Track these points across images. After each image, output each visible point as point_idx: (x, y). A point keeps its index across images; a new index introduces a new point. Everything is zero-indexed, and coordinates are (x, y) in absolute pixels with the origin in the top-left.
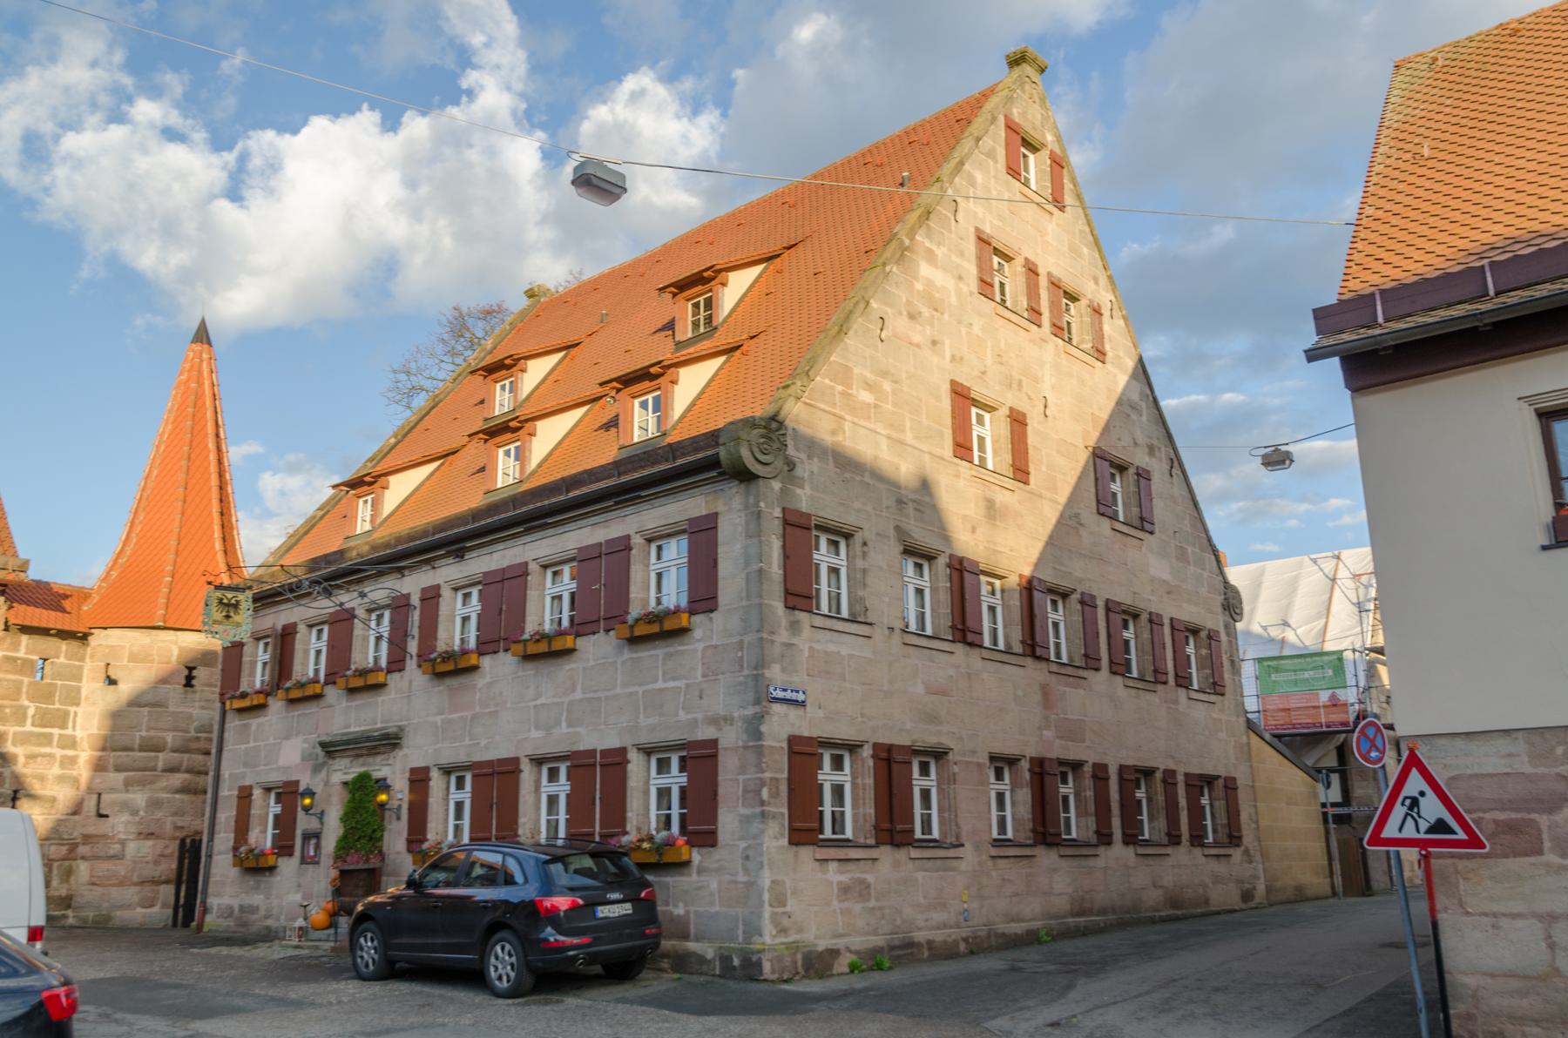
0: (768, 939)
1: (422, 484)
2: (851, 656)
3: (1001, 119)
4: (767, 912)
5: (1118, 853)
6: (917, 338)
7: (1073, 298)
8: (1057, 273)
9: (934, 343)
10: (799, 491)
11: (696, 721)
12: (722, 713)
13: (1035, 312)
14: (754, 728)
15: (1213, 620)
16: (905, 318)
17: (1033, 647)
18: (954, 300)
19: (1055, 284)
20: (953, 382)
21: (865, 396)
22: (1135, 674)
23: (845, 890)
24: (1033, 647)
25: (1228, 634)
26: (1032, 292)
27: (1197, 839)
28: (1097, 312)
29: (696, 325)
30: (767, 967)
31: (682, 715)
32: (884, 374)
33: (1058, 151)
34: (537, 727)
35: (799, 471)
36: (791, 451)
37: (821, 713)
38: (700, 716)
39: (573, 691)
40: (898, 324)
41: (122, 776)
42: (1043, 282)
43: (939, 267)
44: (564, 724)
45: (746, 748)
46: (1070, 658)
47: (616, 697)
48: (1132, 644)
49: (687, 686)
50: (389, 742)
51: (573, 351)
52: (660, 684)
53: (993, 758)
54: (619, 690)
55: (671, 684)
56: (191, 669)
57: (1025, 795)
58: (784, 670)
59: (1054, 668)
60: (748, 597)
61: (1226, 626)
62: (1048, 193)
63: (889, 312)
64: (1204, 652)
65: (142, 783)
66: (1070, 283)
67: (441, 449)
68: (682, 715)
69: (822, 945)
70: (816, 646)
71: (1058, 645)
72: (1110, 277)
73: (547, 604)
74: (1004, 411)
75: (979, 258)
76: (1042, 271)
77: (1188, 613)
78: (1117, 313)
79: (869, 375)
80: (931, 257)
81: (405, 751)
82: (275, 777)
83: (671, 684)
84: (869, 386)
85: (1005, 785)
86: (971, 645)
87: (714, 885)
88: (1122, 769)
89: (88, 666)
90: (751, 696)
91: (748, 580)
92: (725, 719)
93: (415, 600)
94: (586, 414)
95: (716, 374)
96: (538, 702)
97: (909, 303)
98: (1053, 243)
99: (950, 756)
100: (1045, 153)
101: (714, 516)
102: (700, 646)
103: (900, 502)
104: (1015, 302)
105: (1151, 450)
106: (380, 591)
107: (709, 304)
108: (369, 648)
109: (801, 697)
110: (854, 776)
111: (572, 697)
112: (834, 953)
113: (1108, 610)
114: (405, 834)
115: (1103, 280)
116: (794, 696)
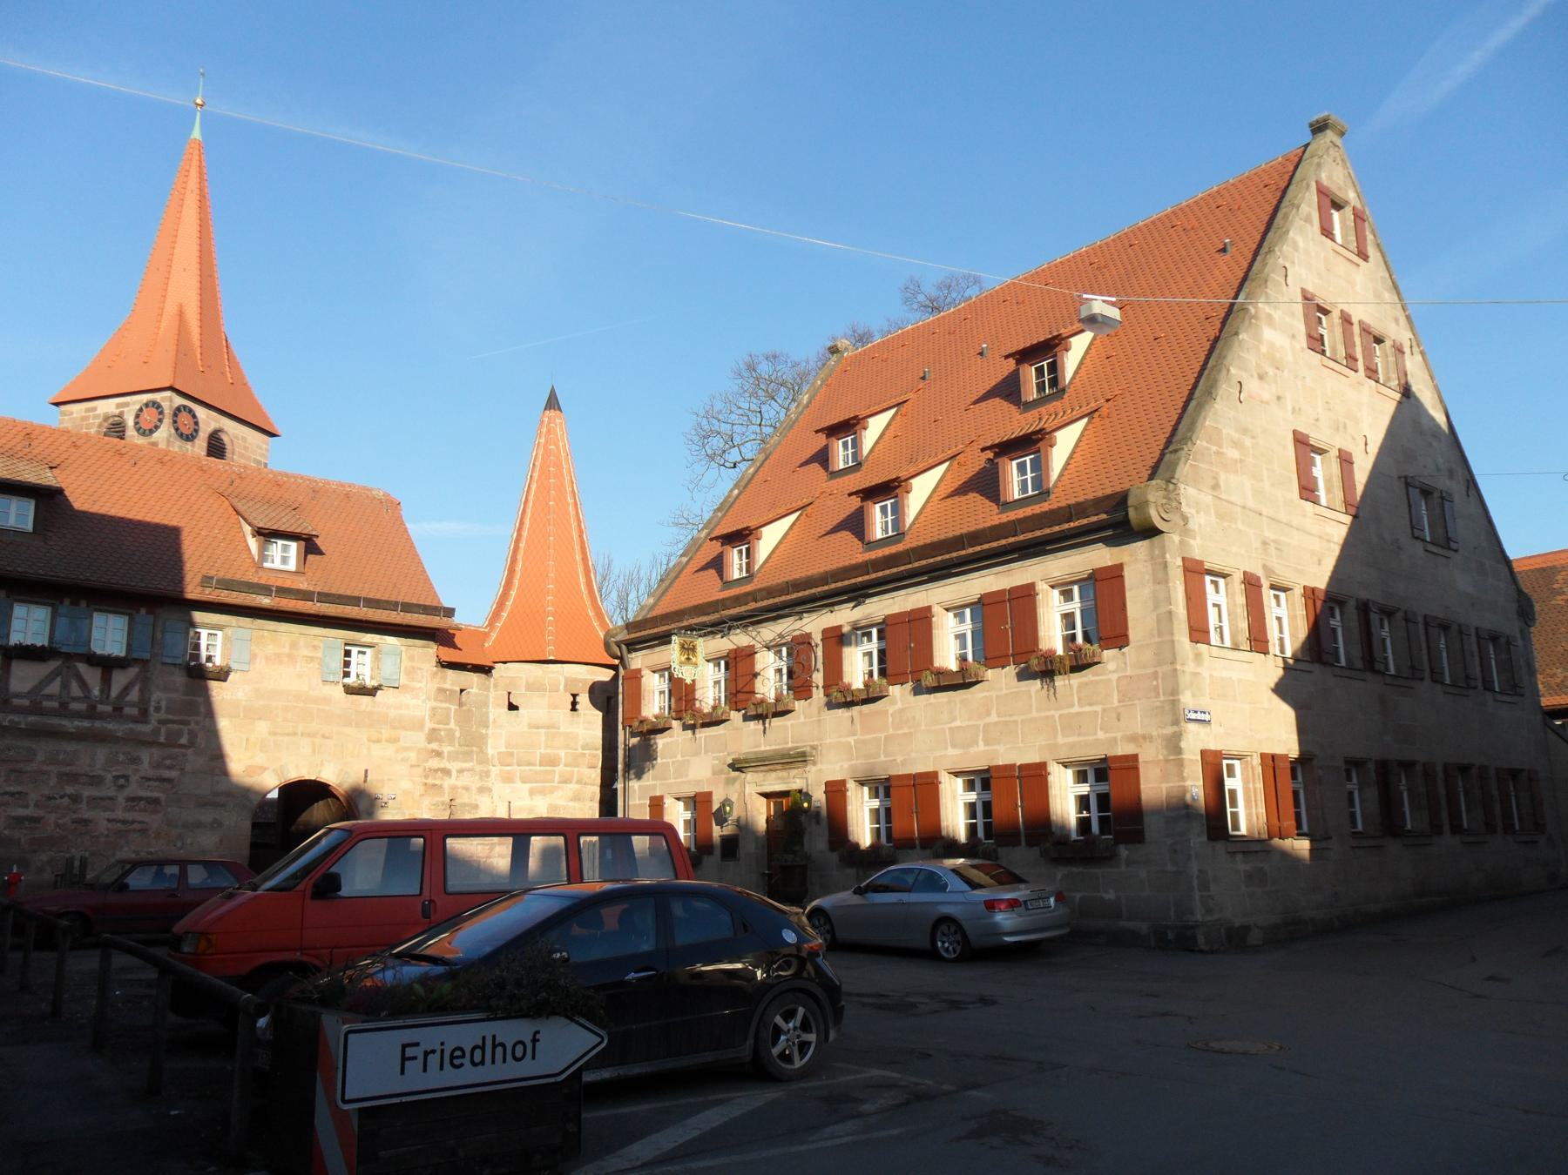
0: (1199, 917)
1: (787, 534)
2: (1240, 680)
3: (1313, 185)
4: (1197, 895)
5: (1448, 841)
6: (1266, 396)
7: (1379, 340)
8: (1368, 320)
9: (1279, 398)
10: (1192, 542)
11: (1115, 739)
12: (1140, 732)
13: (1351, 358)
14: (1174, 745)
15: (1511, 627)
16: (1256, 381)
17: (1370, 662)
18: (1290, 358)
19: (1365, 330)
20: (1295, 432)
21: (1232, 453)
22: (1343, 663)
23: (1249, 876)
24: (1370, 662)
25: (1523, 639)
26: (1348, 342)
27: (1508, 828)
28: (1399, 350)
29: (1041, 387)
30: (1201, 939)
31: (1101, 735)
32: (1245, 431)
33: (1359, 206)
34: (954, 746)
35: (1191, 525)
36: (1184, 508)
37: (1221, 730)
38: (1119, 735)
39: (988, 714)
40: (1252, 385)
41: (528, 786)
42: (1356, 329)
43: (1274, 330)
44: (981, 743)
45: (1167, 761)
46: (1397, 669)
47: (1031, 720)
48: (1340, 631)
49: (1104, 710)
50: (797, 759)
51: (904, 409)
52: (1076, 709)
53: (1347, 762)
54: (1034, 714)
55: (1087, 709)
56: (574, 696)
57: (1372, 793)
58: (1194, 695)
59: (1388, 680)
60: (1160, 634)
61: (1522, 632)
62: (1353, 246)
63: (1244, 377)
64: (1504, 657)
65: (543, 792)
66: (1378, 327)
67: (801, 504)
68: (1101, 735)
69: (1237, 923)
70: (1215, 674)
71: (1281, 640)
72: (1408, 317)
73: (949, 644)
74: (1334, 453)
75: (1306, 316)
76: (1355, 320)
77: (1488, 621)
78: (1416, 349)
79: (1233, 433)
80: (1270, 320)
81: (819, 766)
82: (690, 790)
83: (1087, 709)
84: (1236, 444)
85: (1353, 785)
86: (1325, 664)
87: (1143, 874)
88: (1446, 767)
89: (492, 694)
90: (1169, 718)
91: (1158, 621)
92: (1144, 737)
93: (817, 638)
94: (948, 470)
95: (1082, 435)
96: (954, 725)
97: (1258, 365)
98: (1360, 291)
99: (1315, 762)
100: (1348, 211)
101: (1120, 567)
102: (1115, 677)
103: (1265, 543)
104: (1334, 350)
105: (1451, 474)
106: (786, 627)
107: (1053, 368)
108: (769, 681)
109: (1207, 717)
110: (1245, 781)
111: (987, 720)
112: (1246, 929)
113: (1426, 624)
114: (826, 837)
115: (1403, 320)
116: (1202, 717)
